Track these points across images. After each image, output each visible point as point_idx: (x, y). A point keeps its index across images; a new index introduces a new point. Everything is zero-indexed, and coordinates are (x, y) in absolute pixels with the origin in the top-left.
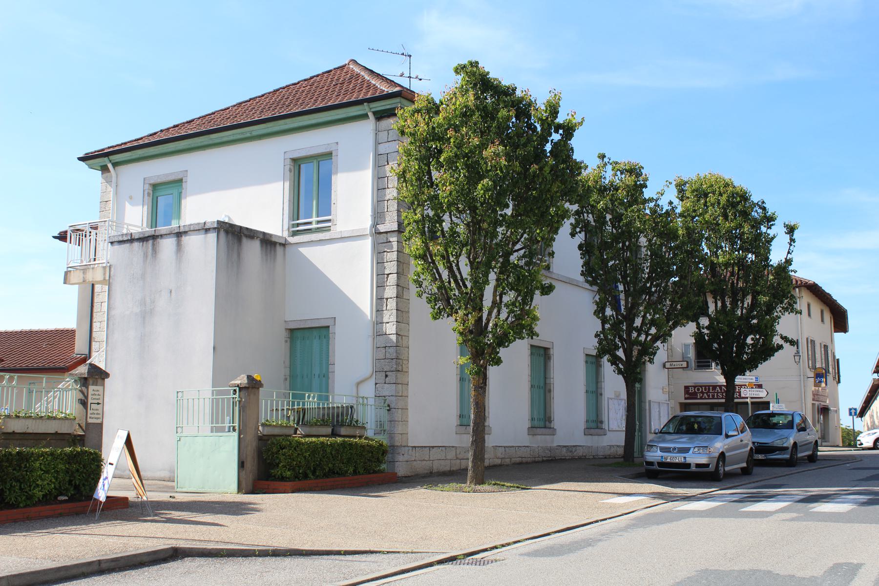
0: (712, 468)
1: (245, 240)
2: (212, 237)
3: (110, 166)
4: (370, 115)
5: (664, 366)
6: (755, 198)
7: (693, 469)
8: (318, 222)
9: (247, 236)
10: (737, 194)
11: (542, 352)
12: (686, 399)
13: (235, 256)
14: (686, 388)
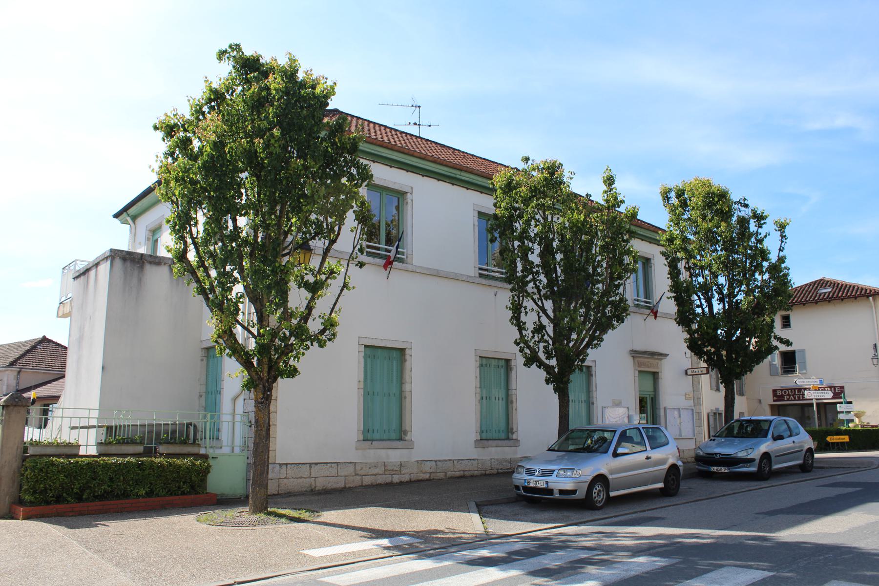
0: (581, 494)
1: (148, 267)
5: (686, 374)
6: (735, 197)
7: (557, 495)
9: (150, 263)
10: (713, 193)
11: (503, 363)
12: (774, 401)
13: (135, 281)
14: (774, 391)
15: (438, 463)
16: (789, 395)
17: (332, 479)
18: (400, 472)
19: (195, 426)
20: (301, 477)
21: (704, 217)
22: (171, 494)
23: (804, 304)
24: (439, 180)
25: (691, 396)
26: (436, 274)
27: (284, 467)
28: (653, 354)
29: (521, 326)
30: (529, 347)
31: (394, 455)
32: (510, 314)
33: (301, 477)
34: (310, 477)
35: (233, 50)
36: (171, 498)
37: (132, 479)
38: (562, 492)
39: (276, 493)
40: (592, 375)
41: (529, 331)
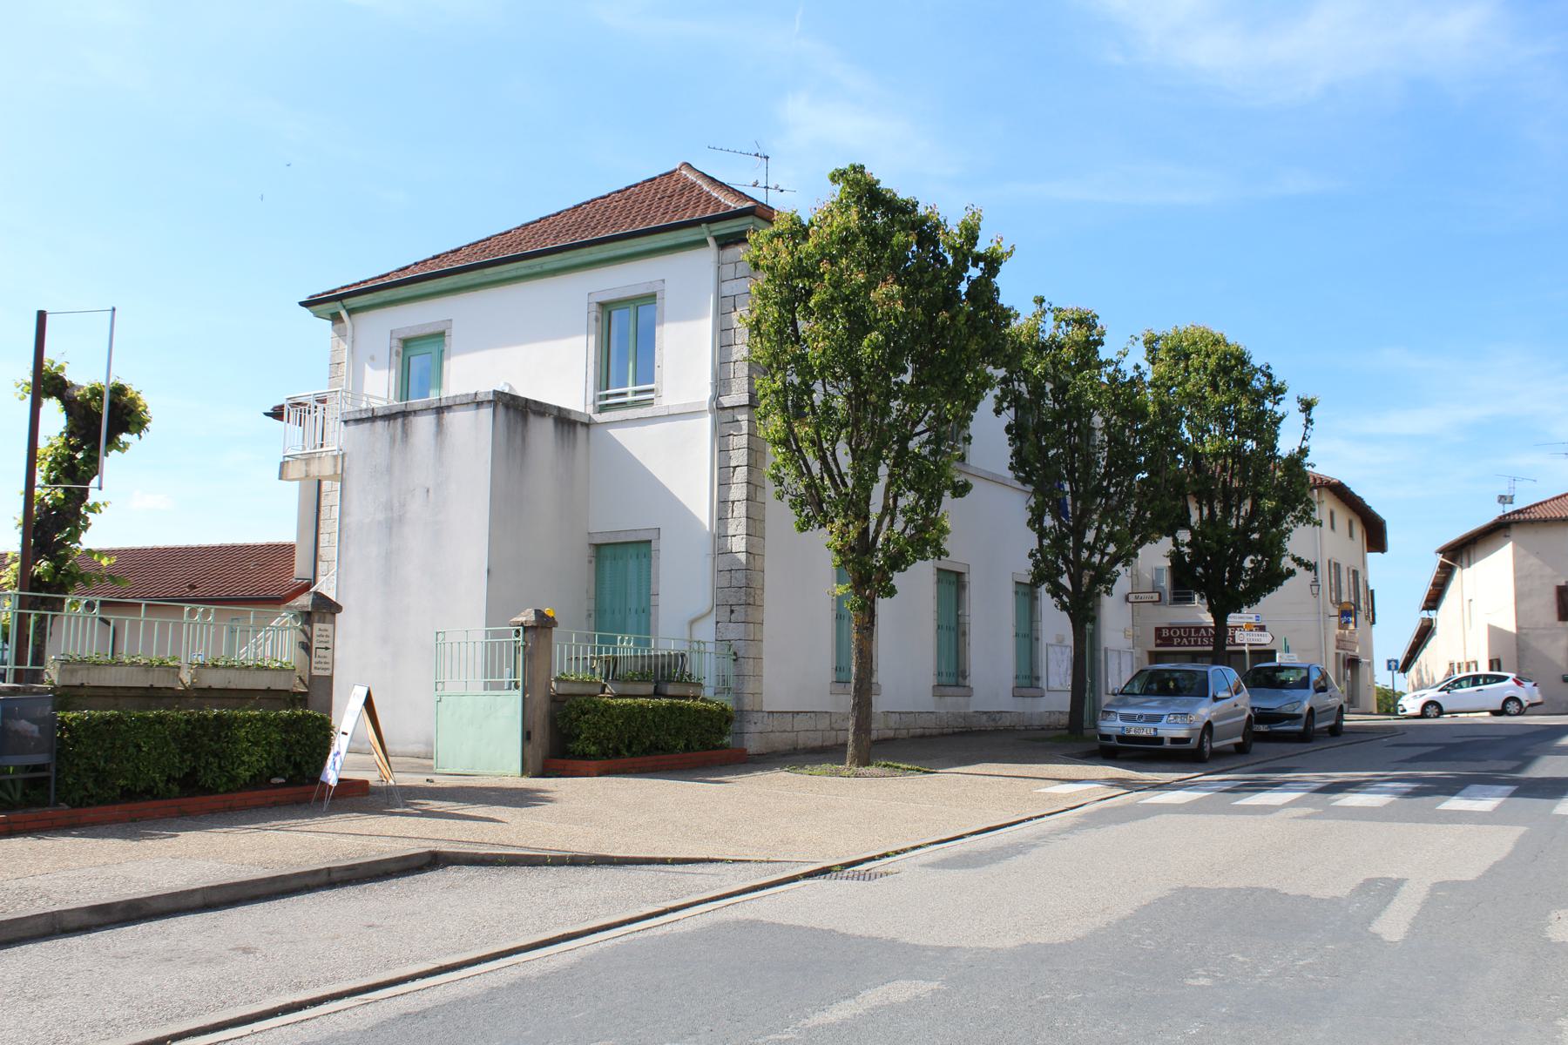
0: (1193, 744)
1: (532, 419)
2: (486, 413)
3: (344, 314)
4: (710, 240)
5: (1127, 599)
7: (1167, 745)
8: (636, 393)
10: (1231, 354)
11: (953, 578)
14: (1158, 630)
16: (1181, 637)
21: (1215, 387)
38: (1174, 740)
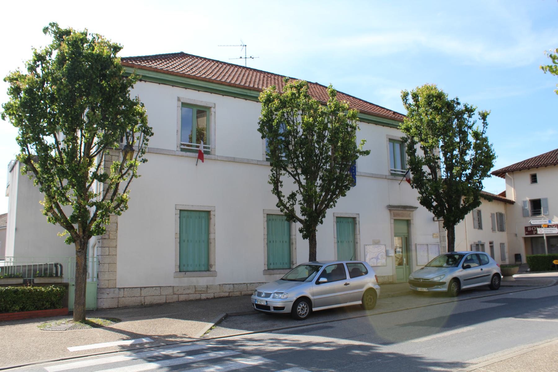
7: (272, 310)
10: (432, 95)
12: (526, 234)
15: (235, 286)
17: (156, 298)
18: (206, 292)
19: (61, 265)
20: (134, 297)
22: (38, 309)
23: (546, 166)
24: (235, 97)
25: (438, 235)
26: (233, 160)
27: (122, 290)
28: (405, 207)
29: (278, 194)
30: (287, 208)
31: (202, 281)
32: (272, 187)
33: (134, 297)
34: (141, 296)
35: (53, 26)
36: (37, 311)
37: (10, 301)
38: (275, 308)
39: (116, 307)
40: (356, 224)
41: (286, 198)
